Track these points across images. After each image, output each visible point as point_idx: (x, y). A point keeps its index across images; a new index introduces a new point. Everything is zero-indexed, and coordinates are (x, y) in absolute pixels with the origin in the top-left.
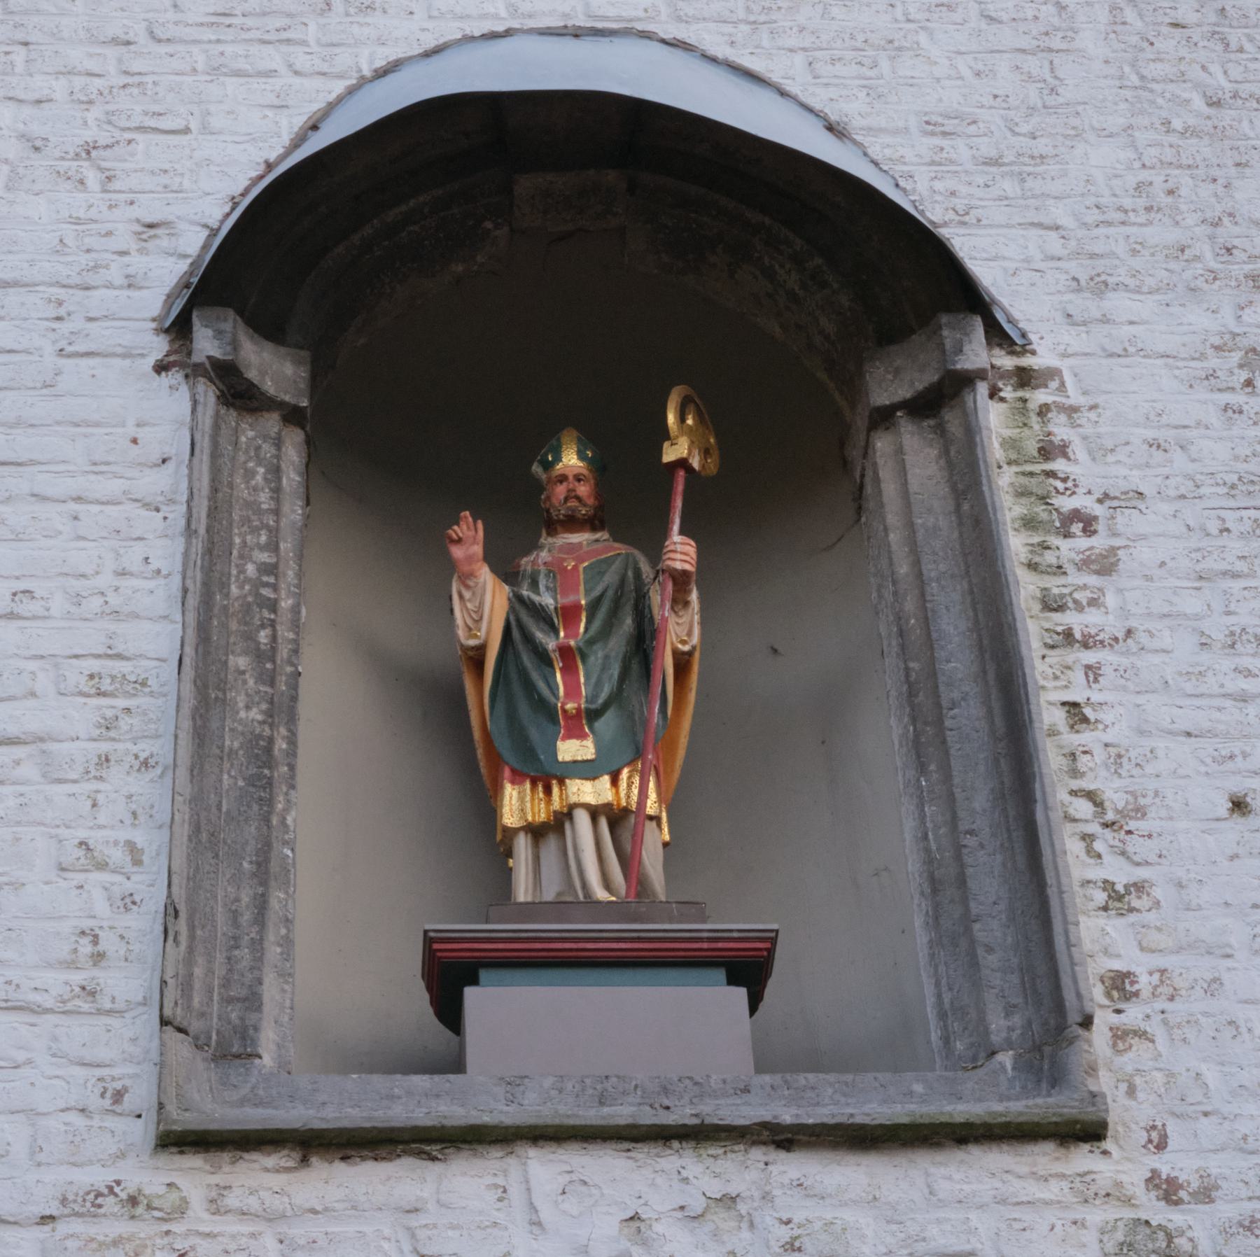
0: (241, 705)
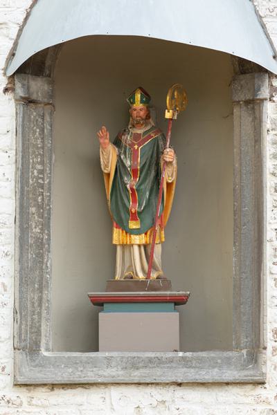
0: (34, 226)
